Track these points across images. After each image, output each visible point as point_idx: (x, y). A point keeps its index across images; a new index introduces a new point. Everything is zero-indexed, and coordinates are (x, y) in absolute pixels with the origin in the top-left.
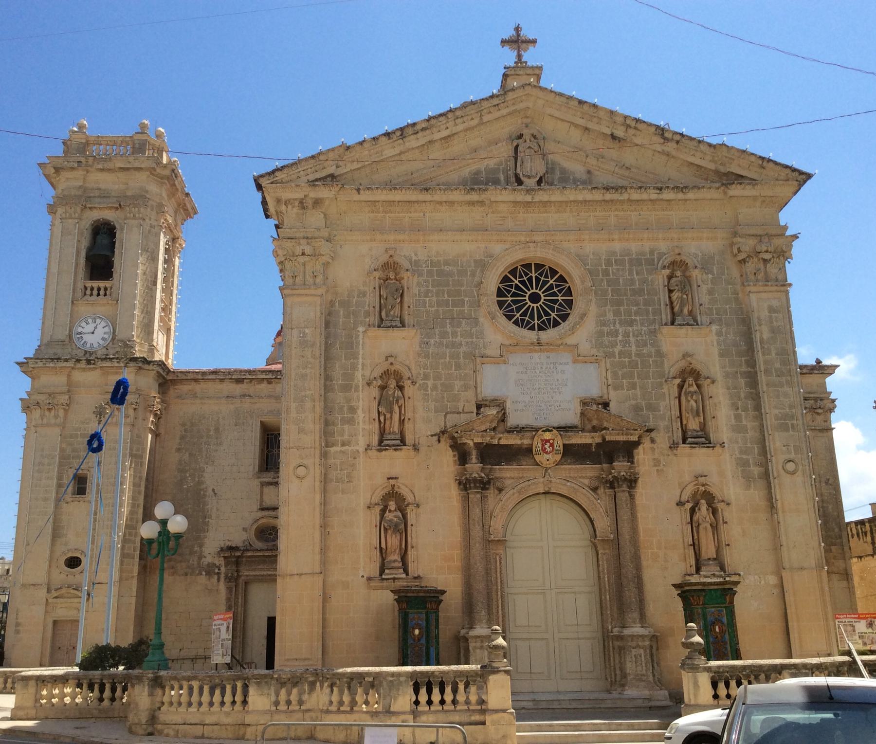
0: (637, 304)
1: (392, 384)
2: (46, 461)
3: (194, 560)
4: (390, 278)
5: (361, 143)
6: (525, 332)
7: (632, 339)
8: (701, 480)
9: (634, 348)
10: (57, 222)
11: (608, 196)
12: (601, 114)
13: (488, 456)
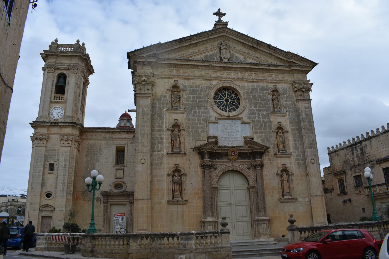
0: (262, 104)
2: (39, 159)
7: (261, 116)
8: (284, 166)
9: (261, 119)
10: (46, 74)
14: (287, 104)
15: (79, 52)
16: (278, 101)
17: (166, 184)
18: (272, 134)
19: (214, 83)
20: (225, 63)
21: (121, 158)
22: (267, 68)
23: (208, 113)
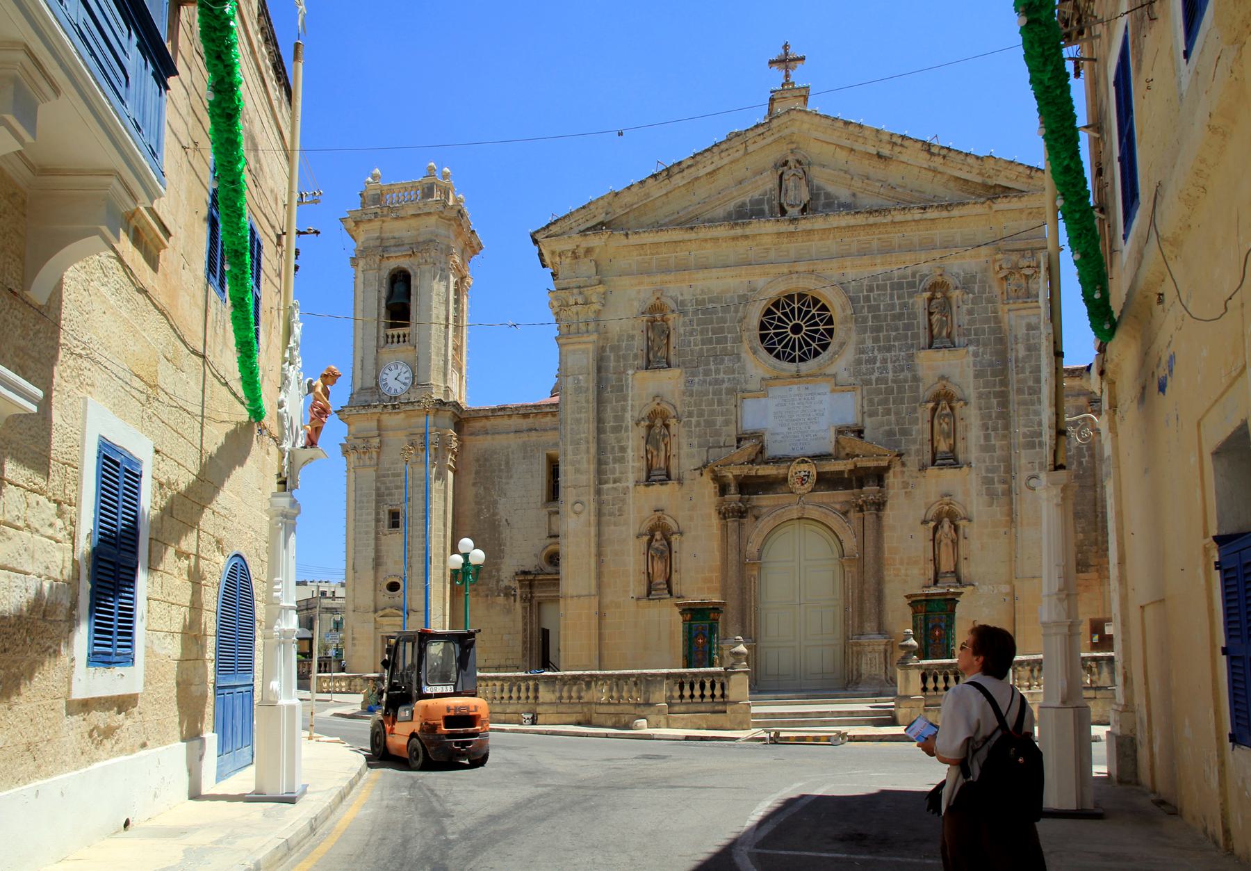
0: (897, 329)
1: (658, 422)
2: (365, 499)
3: (492, 584)
4: (656, 323)
5: (629, 188)
6: (785, 365)
7: (890, 366)
10: (360, 275)
11: (871, 220)
12: (867, 133)
13: (748, 488)
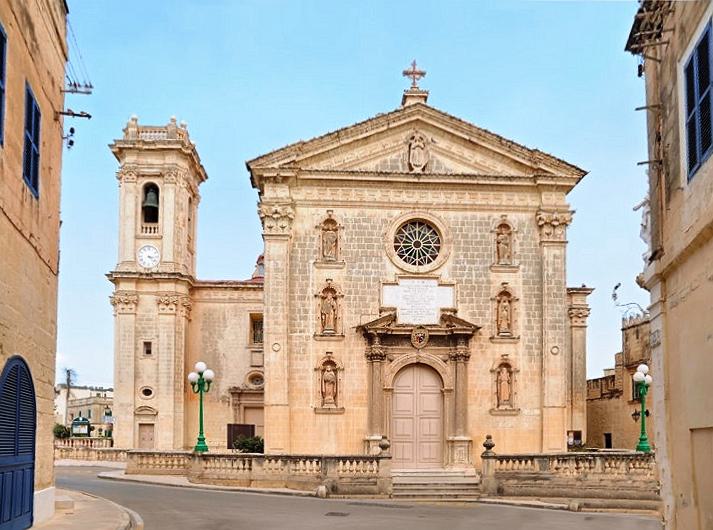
9: (474, 278)
14: (522, 250)
15: (177, 142)
16: (507, 245)
17: (312, 381)
18: (490, 304)
19: (396, 213)
20: (417, 175)
21: (259, 332)
22: (492, 182)
23: (384, 266)
